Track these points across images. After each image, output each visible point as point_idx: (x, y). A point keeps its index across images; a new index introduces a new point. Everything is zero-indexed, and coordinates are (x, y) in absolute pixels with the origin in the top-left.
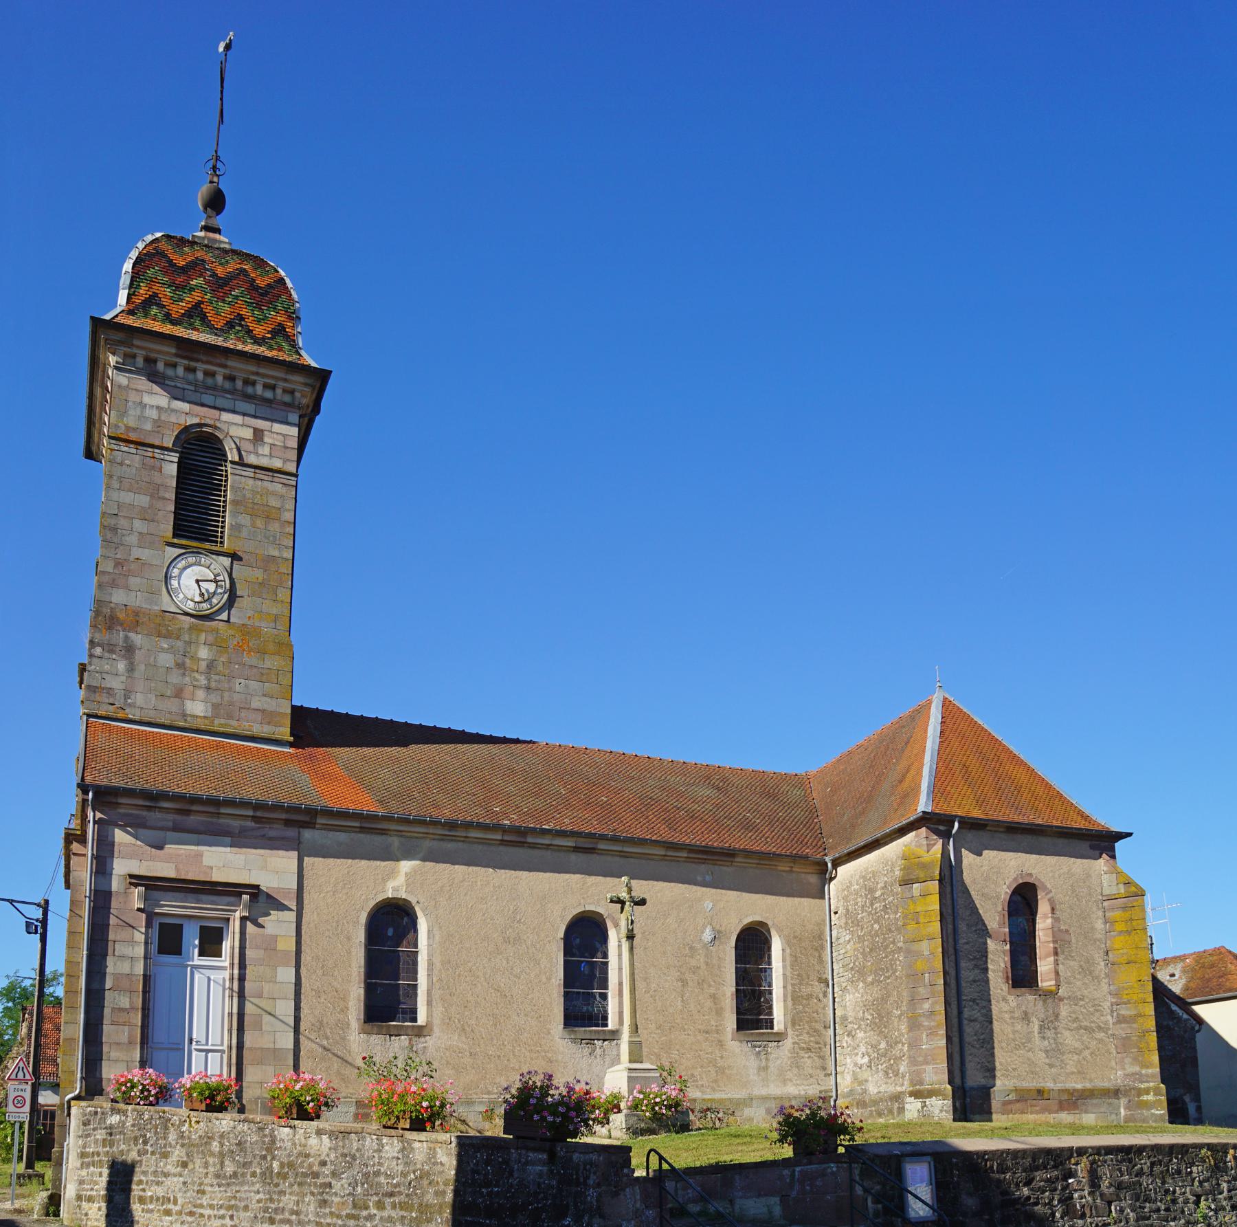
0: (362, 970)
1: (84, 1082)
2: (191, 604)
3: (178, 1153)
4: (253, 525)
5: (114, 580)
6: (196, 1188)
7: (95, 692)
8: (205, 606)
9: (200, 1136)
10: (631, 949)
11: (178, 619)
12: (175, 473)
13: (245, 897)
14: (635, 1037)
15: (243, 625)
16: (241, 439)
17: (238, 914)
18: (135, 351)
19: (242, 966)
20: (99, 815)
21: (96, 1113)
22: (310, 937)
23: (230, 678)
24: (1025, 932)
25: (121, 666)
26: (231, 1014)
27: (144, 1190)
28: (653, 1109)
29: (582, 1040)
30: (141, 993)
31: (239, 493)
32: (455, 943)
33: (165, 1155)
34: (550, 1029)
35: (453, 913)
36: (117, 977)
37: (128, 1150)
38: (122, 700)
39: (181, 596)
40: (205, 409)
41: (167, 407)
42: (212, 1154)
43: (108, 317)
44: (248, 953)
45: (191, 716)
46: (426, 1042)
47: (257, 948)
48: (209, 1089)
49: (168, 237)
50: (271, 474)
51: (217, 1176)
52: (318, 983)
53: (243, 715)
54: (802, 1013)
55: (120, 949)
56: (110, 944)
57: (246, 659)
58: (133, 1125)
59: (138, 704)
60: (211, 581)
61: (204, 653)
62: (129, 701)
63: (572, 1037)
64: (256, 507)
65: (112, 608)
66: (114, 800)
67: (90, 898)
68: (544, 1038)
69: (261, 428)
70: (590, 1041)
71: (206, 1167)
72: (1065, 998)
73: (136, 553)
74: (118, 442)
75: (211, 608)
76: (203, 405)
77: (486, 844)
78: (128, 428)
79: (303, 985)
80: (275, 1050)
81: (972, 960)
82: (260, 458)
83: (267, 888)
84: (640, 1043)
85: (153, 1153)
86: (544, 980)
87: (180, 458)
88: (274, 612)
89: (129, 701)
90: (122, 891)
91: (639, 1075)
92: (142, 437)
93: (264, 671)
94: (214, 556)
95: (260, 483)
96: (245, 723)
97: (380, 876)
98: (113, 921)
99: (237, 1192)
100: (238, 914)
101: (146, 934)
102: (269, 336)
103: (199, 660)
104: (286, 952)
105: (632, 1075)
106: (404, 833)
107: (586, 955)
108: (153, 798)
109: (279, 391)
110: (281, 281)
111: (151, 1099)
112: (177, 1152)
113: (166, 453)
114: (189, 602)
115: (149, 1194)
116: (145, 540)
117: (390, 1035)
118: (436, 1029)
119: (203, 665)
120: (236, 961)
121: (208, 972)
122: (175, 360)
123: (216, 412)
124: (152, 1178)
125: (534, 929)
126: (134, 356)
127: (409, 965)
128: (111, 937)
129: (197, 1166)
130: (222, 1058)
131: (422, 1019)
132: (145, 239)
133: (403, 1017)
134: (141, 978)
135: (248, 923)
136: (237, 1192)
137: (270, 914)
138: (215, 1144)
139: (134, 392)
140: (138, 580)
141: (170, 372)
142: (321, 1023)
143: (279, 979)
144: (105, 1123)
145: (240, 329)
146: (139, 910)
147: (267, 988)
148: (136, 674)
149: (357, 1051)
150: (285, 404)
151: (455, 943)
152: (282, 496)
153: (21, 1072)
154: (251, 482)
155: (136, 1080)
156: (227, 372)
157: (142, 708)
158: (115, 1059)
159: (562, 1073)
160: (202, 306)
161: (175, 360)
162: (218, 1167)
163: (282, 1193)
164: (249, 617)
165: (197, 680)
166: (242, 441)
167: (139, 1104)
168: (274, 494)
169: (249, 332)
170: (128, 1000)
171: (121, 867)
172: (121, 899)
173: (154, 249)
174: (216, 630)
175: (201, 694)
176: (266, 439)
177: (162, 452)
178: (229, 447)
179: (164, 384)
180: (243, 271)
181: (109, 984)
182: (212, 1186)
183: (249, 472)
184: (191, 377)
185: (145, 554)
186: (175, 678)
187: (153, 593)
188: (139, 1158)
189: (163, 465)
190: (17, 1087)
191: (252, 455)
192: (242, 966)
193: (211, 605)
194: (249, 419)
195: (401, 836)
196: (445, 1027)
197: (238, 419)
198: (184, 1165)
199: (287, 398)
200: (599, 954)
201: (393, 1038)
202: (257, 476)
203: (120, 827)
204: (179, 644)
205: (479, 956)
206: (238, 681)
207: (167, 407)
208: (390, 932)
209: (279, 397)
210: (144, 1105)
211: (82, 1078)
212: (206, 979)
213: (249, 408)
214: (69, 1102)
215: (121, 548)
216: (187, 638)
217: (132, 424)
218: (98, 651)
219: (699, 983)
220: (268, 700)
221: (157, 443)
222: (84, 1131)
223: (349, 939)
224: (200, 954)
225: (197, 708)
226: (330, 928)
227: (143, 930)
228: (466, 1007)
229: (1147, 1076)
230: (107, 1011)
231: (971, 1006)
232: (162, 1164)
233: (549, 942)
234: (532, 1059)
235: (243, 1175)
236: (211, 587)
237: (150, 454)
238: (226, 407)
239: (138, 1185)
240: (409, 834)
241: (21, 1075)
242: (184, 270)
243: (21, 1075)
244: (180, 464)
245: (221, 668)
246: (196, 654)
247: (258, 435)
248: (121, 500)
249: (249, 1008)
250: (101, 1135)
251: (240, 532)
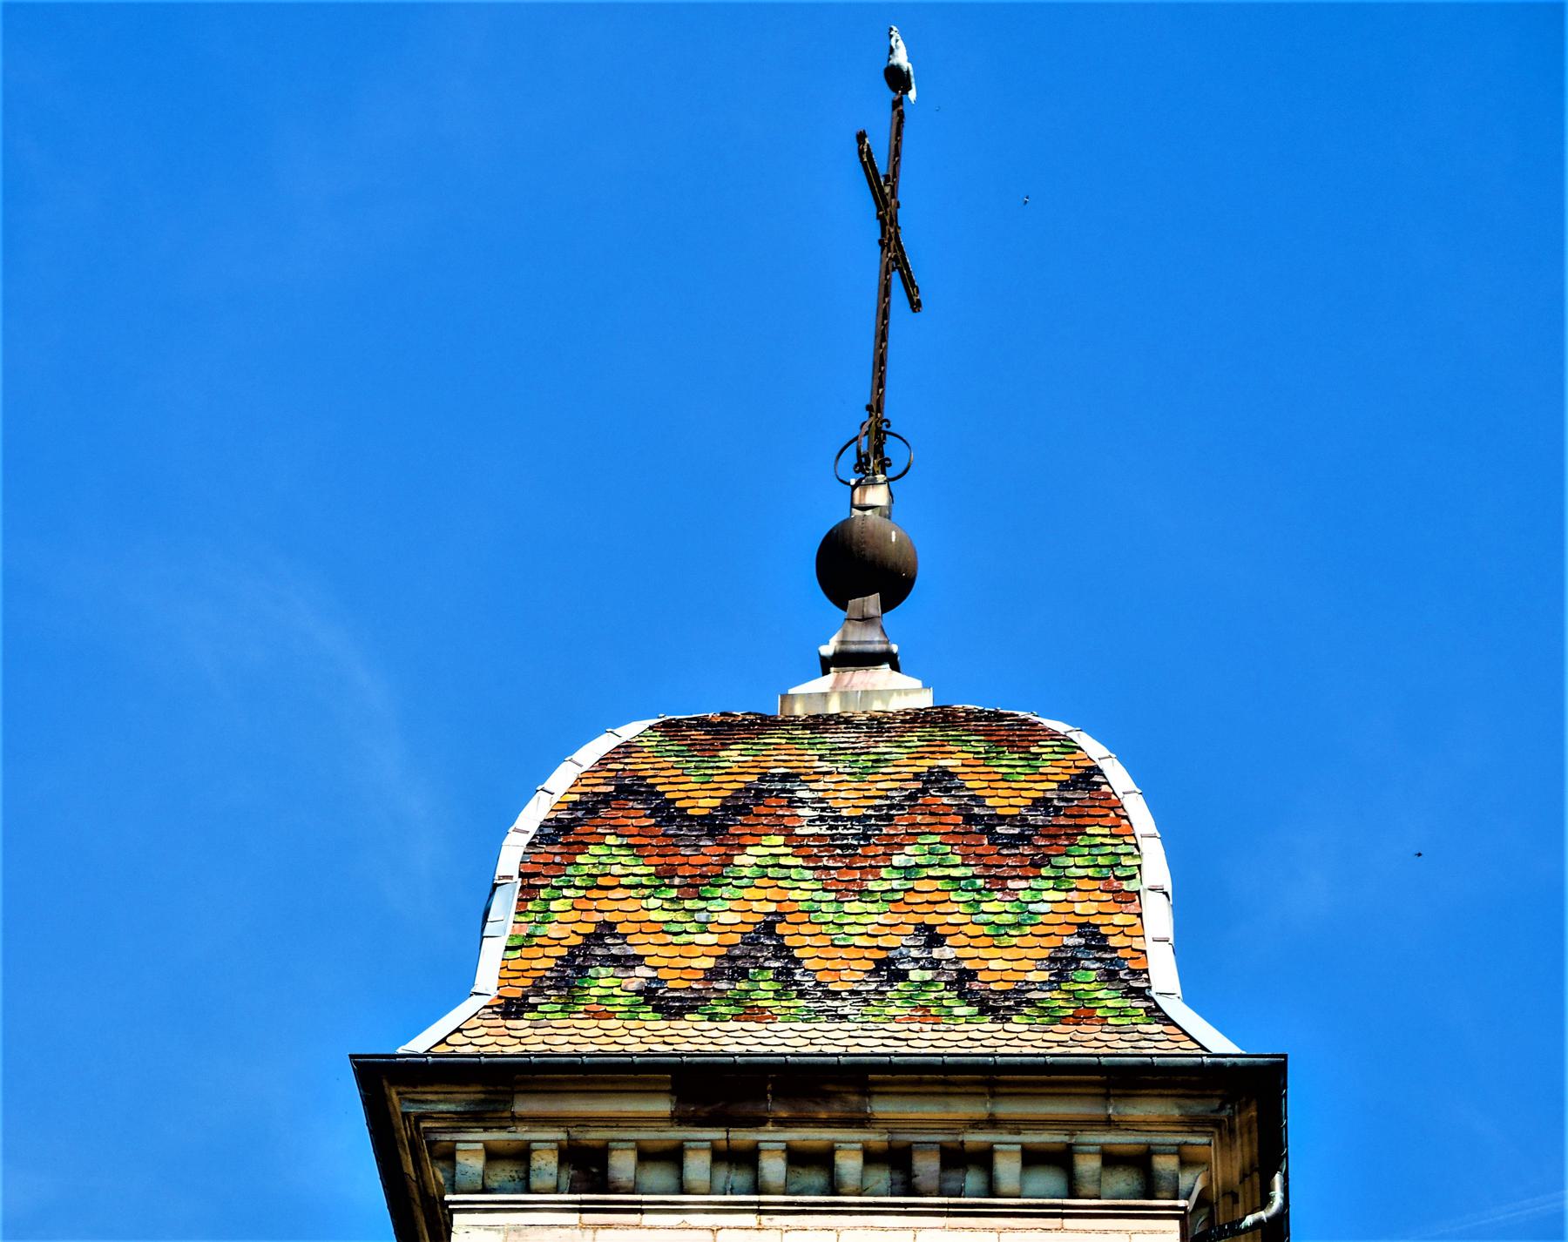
11: (1223, 1179)
18: (523, 1134)
43: (419, 1044)
49: (670, 729)
110: (1088, 777)
126: (522, 1155)
132: (546, 786)
145: (928, 975)
156: (876, 1138)
242: (712, 825)
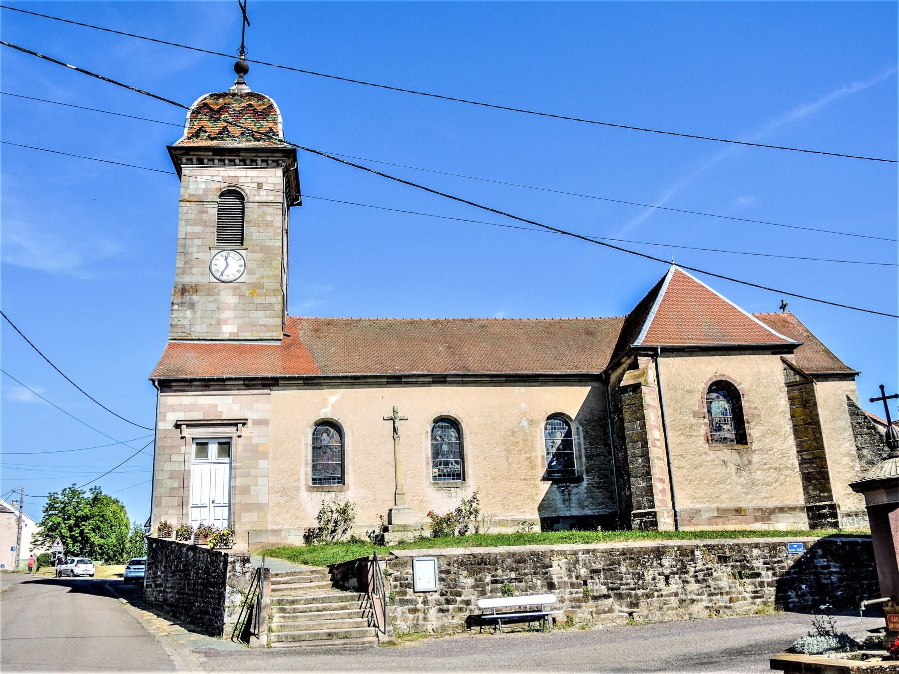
5: (184, 271)
18: (191, 157)
24: (726, 410)
54: (593, 465)
62: (193, 330)
66: (169, 384)
69: (261, 182)
72: (757, 450)
73: (196, 256)
77: (379, 384)
78: (190, 195)
80: (257, 504)
81: (679, 431)
95: (261, 210)
110: (271, 106)
122: (213, 157)
147: (253, 471)
156: (241, 158)
161: (213, 157)
164: (257, 279)
173: (202, 104)
180: (250, 105)
185: (201, 255)
202: (260, 207)
217: (192, 192)
219: (518, 451)
220: (268, 319)
229: (824, 497)
231: (679, 459)
242: (218, 111)
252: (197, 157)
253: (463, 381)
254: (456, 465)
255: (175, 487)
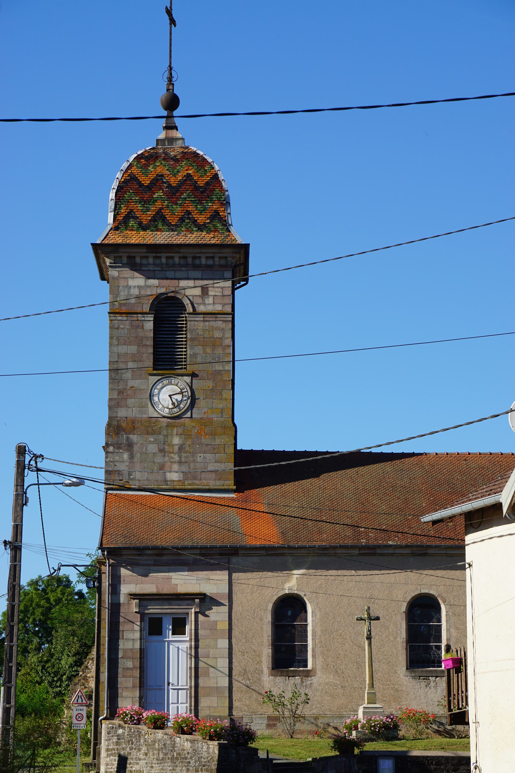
0: (270, 638)
1: (109, 710)
2: (167, 410)
3: (144, 749)
4: (205, 352)
5: (118, 403)
6: (150, 765)
7: (110, 474)
8: (175, 410)
9: (152, 741)
10: (370, 644)
12: (152, 328)
13: (197, 601)
14: (371, 690)
15: (201, 418)
16: (194, 296)
17: (193, 610)
18: (121, 254)
19: (197, 640)
20: (111, 561)
21: (113, 727)
22: (237, 620)
23: (194, 454)
25: (126, 456)
26: (191, 668)
27: (132, 767)
28: (371, 729)
29: (420, 677)
30: (139, 659)
31: (194, 333)
32: (330, 619)
33: (139, 750)
34: (397, 670)
35: (328, 600)
36: (125, 651)
37: (126, 747)
38: (127, 477)
39: (160, 406)
40: (168, 281)
41: (144, 285)
42: (156, 750)
44: (200, 632)
45: (170, 481)
46: (312, 680)
47: (205, 629)
48: (154, 718)
50: (214, 316)
51: (157, 760)
52: (243, 648)
53: (203, 476)
55: (127, 635)
56: (121, 633)
57: (203, 440)
58: (128, 735)
59: (137, 478)
60: (179, 394)
61: (176, 441)
62: (132, 477)
63: (413, 675)
64: (206, 340)
65: (118, 421)
67: (108, 609)
68: (392, 676)
70: (426, 678)
71: (154, 756)
73: (131, 383)
74: (115, 315)
75: (180, 411)
76: (167, 279)
79: (234, 649)
80: (217, 687)
82: (207, 306)
83: (210, 594)
84: (374, 693)
85: (135, 749)
86: (392, 639)
87: (154, 318)
88: (221, 407)
89: (132, 477)
90: (126, 602)
91: (370, 710)
92: (130, 308)
93: (216, 447)
94: (180, 377)
95: (207, 323)
96: (204, 481)
97: (280, 581)
98: (121, 620)
99: (163, 766)
100: (193, 610)
101: (141, 626)
102: (208, 221)
103: (173, 445)
104: (223, 631)
105: (366, 710)
106: (294, 554)
107: (425, 621)
108: (140, 550)
109: (217, 260)
111: (135, 721)
112: (144, 748)
113: (145, 316)
114: (166, 409)
115: (134, 769)
116: (137, 373)
117: (289, 677)
118: (319, 673)
119: (176, 448)
120: (193, 637)
121: (177, 645)
123: (176, 281)
124: (135, 761)
125: (384, 607)
127: (302, 632)
128: (121, 628)
129: (151, 755)
130: (187, 692)
131: (310, 666)
133: (298, 665)
134: (139, 650)
135: (200, 615)
136: (163, 766)
137: (212, 609)
138: (157, 744)
139: (123, 279)
140: (133, 400)
141: (144, 261)
142: (245, 671)
143: (219, 646)
144: (117, 733)
146: (136, 612)
147: (212, 651)
148: (135, 460)
149: (268, 686)
150: (221, 266)
151: (330, 619)
152: (223, 329)
153: (80, 699)
154: (201, 324)
155: (127, 712)
156: (181, 255)
157: (139, 480)
158: (125, 696)
159: (406, 698)
160: (162, 211)
162: (157, 755)
163: (177, 766)
164: (205, 413)
165: (173, 458)
166: (194, 298)
167: (130, 724)
168: (217, 329)
169: (195, 222)
170: (132, 663)
171: (125, 589)
172: (126, 607)
174: (184, 425)
175: (176, 467)
176: (210, 293)
177: (143, 316)
178: (186, 302)
179: (141, 270)
181: (120, 655)
182: (155, 764)
183: (200, 318)
184: (158, 261)
185: (136, 383)
186: (159, 459)
187: (142, 407)
188: (130, 751)
189: (144, 324)
190: (78, 708)
191: (202, 306)
192: (197, 640)
193: (179, 409)
194: (198, 281)
195: (293, 556)
196: (324, 671)
197: (191, 283)
198: (146, 754)
199: (223, 262)
200: (435, 620)
201: (290, 678)
202: (206, 319)
203: (124, 567)
204: (161, 437)
205: (346, 626)
206: (199, 455)
207: (144, 285)
208: (289, 613)
209: (217, 263)
210: (132, 724)
211: (107, 708)
212: (177, 649)
213: (198, 274)
214: (101, 721)
215: (122, 382)
216: (165, 432)
218: (111, 449)
220: (219, 464)
221: (139, 310)
222: (108, 737)
223: (261, 620)
224: (173, 634)
225: (174, 476)
226: (249, 614)
227: (139, 624)
228: (338, 658)
230: (120, 670)
232: (138, 754)
233: (395, 614)
234: (384, 689)
235: (165, 758)
236: (179, 397)
237: (135, 319)
238: (182, 277)
239: (130, 765)
240: (298, 554)
241: (80, 701)
243: (80, 701)
244: (155, 321)
245: (187, 448)
246: (171, 442)
247: (205, 290)
248: (119, 352)
249: (201, 665)
250: (115, 739)
251: (196, 358)
252: (127, 255)
253: (446, 554)
254: (436, 650)
255: (129, 667)
